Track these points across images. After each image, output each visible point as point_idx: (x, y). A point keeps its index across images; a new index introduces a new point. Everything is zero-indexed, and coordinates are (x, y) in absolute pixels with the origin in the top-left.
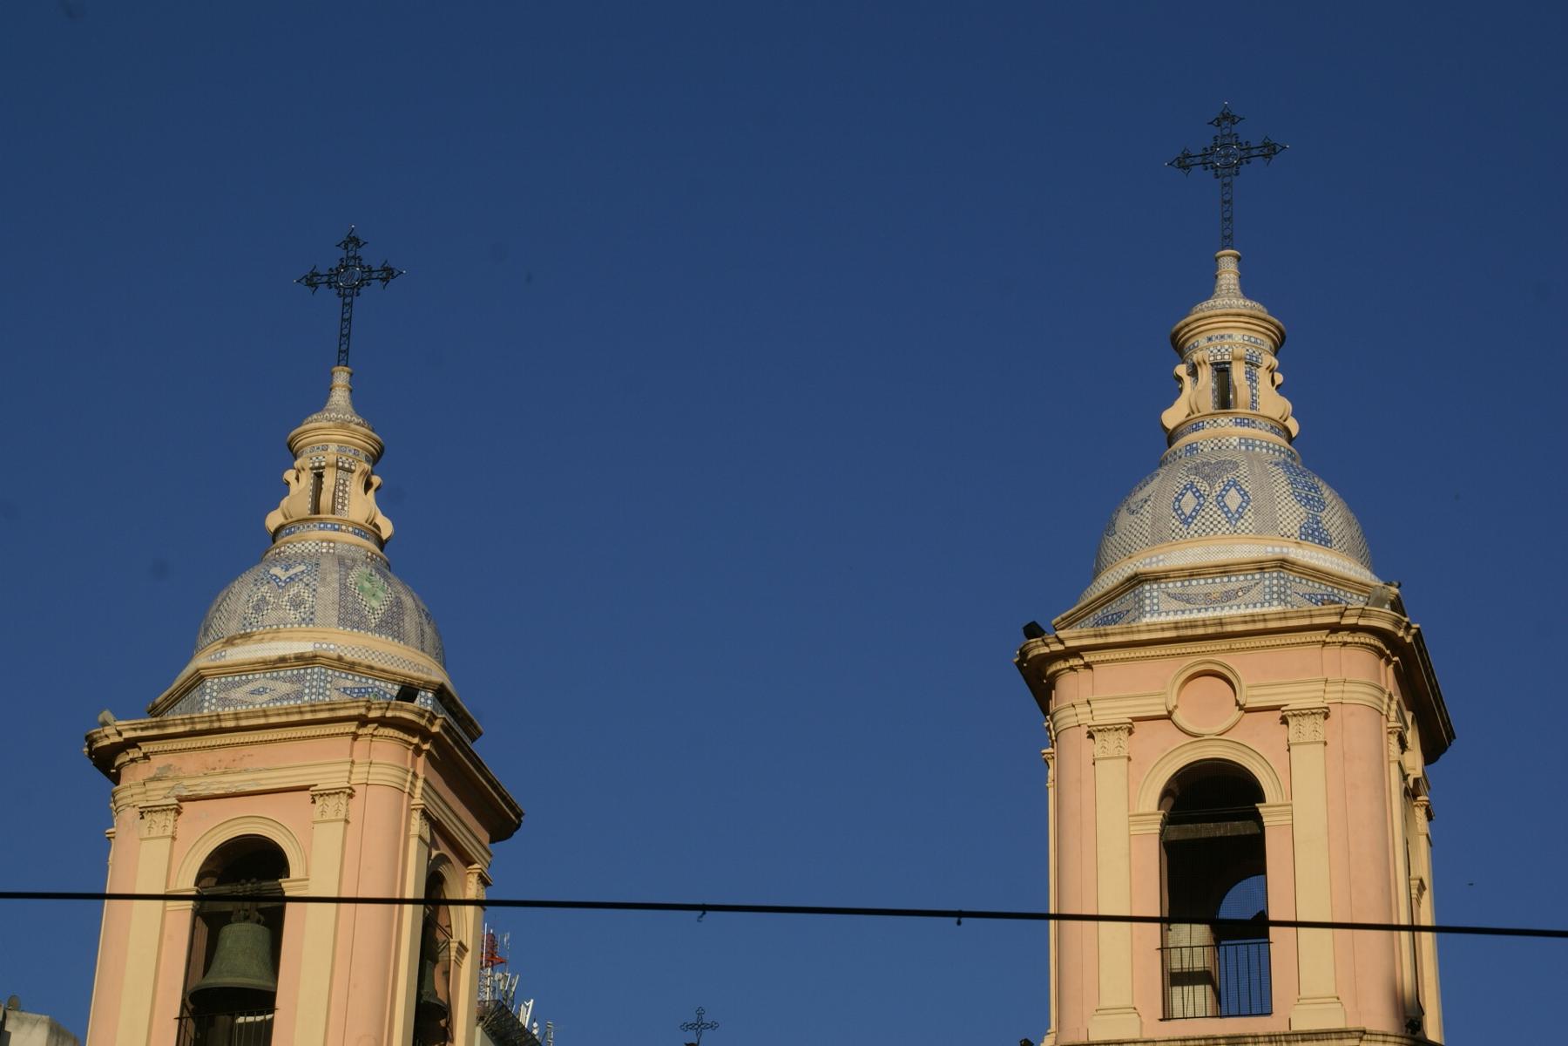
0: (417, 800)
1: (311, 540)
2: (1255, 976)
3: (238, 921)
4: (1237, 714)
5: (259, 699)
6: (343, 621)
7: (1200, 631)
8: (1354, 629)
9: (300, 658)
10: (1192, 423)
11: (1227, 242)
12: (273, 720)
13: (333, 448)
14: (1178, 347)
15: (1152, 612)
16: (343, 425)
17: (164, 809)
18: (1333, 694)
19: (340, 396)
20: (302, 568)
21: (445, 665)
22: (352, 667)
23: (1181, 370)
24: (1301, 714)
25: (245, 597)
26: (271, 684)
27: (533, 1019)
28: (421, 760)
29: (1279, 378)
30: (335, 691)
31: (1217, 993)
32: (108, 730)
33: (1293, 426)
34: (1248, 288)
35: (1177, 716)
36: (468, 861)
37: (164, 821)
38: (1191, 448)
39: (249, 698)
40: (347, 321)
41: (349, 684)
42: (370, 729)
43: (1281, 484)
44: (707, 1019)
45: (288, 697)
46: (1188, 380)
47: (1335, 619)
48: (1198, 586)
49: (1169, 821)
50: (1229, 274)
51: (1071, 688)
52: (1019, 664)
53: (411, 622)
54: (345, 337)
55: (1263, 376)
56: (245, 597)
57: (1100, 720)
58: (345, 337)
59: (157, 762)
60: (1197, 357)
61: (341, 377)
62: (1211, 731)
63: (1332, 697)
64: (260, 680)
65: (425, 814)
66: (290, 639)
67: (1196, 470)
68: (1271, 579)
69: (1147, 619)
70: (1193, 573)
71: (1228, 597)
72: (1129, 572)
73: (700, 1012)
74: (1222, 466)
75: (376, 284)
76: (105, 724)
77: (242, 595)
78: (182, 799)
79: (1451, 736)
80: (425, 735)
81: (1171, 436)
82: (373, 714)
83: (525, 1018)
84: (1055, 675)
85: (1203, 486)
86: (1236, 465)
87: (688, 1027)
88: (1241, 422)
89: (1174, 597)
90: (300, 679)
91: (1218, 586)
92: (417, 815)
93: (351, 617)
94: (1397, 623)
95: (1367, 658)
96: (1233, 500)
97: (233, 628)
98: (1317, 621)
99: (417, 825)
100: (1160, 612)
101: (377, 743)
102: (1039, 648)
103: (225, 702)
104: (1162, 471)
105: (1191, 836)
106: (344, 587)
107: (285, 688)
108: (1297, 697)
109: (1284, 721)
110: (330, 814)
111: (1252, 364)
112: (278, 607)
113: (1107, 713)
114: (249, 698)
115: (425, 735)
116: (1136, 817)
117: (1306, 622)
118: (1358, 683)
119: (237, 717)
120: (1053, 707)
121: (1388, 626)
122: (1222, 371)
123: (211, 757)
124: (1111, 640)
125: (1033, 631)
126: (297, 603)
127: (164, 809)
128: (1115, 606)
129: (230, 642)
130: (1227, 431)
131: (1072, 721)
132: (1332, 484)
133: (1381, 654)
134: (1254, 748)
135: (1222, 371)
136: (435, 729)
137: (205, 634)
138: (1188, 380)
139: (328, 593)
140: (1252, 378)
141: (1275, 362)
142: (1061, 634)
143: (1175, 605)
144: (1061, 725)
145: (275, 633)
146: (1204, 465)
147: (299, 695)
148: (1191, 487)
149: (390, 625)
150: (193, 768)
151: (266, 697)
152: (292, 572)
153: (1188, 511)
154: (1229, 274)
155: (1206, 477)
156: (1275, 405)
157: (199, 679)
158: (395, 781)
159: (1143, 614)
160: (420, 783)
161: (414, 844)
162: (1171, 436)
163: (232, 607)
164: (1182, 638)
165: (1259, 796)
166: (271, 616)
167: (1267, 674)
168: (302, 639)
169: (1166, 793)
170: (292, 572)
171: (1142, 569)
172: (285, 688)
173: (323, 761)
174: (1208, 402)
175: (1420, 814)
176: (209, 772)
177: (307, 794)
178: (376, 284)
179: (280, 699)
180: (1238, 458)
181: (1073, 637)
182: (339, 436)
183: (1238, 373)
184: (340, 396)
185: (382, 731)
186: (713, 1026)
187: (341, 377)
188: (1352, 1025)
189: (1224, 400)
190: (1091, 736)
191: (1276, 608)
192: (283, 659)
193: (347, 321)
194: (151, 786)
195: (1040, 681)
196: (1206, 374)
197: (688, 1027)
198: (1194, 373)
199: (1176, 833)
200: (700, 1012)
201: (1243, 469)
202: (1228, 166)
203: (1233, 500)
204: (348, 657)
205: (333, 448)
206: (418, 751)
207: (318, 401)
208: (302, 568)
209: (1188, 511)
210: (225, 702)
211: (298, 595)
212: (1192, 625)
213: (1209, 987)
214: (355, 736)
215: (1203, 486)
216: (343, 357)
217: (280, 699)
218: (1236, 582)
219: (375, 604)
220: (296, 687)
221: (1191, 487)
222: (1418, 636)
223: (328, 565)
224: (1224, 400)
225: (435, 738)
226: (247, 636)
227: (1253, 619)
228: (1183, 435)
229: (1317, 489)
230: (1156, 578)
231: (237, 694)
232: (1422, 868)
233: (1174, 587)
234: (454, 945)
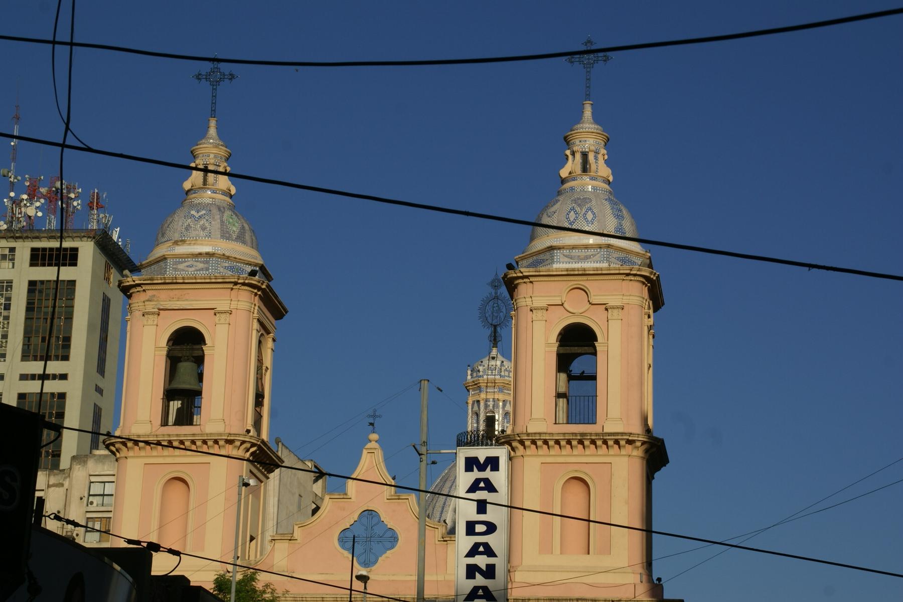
0: (256, 315)
1: (207, 196)
2: (591, 414)
3: (185, 361)
4: (588, 305)
5: (190, 269)
6: (223, 237)
7: (576, 273)
8: (635, 275)
9: (207, 254)
10: (572, 177)
11: (588, 97)
12: (199, 281)
13: (212, 156)
14: (567, 141)
15: (557, 262)
16: (216, 146)
17: (153, 313)
18: (626, 300)
19: (212, 131)
20: (204, 212)
21: (258, 249)
22: (228, 258)
23: (568, 152)
24: (613, 308)
25: (180, 223)
26: (195, 264)
27: (119, 237)
28: (257, 297)
29: (606, 157)
30: (221, 270)
31: (568, 401)
32: (129, 279)
33: (611, 179)
34: (596, 119)
35: (566, 305)
36: (268, 333)
37: (152, 319)
38: (572, 189)
39: (186, 269)
40: (214, 96)
41: (227, 265)
42: (238, 287)
43: (607, 207)
44: (377, 414)
45: (202, 269)
46: (570, 157)
47: (628, 272)
48: (575, 252)
49: (560, 346)
50: (588, 112)
51: (524, 290)
52: (503, 278)
53: (248, 236)
54: (213, 104)
55: (600, 157)
56: (180, 223)
57: (535, 305)
58: (213, 104)
59: (149, 293)
60: (575, 149)
61: (213, 123)
62: (578, 312)
63: (625, 301)
64: (190, 262)
65: (259, 320)
66: (202, 244)
67: (575, 201)
68: (604, 252)
69: (555, 266)
70: (574, 247)
71: (586, 258)
72: (548, 244)
73: (375, 411)
74: (586, 200)
75: (227, 81)
76: (127, 277)
77: (179, 222)
78: (160, 309)
79: (663, 304)
80: (259, 288)
81: (563, 181)
82: (240, 281)
83: (115, 237)
84: (518, 284)
85: (578, 209)
86: (591, 200)
87: (370, 416)
88: (592, 179)
89: (566, 256)
90: (207, 262)
91: (583, 253)
92: (255, 321)
93: (226, 235)
94: (651, 273)
95: (639, 285)
96: (590, 216)
97: (177, 236)
98: (621, 272)
99: (256, 325)
100: (560, 264)
101: (241, 292)
102: (512, 274)
103: (176, 269)
104: (561, 198)
105: (568, 352)
106: (222, 222)
107: (201, 266)
108: (612, 301)
109: (606, 309)
110: (222, 321)
111: (597, 153)
112: (196, 230)
113: (540, 302)
114: (186, 270)
115: (259, 288)
116: (548, 344)
117: (617, 272)
118: (634, 295)
119: (183, 278)
120: (515, 297)
121: (647, 274)
122: (585, 155)
123: (172, 293)
124: (541, 273)
125: (510, 267)
126: (203, 228)
127: (153, 313)
128: (541, 257)
129: (176, 243)
130: (588, 185)
131: (524, 304)
132: (630, 210)
133: (643, 283)
134: (594, 320)
135: (585, 155)
136: (264, 287)
137: (163, 235)
138: (570, 157)
139: (216, 224)
140: (596, 158)
141: (605, 152)
142: (522, 270)
143: (566, 259)
144: (519, 305)
145: (195, 241)
146: (579, 199)
147: (207, 269)
148: (573, 209)
149: (240, 238)
150: (165, 297)
151: (193, 269)
152: (200, 214)
153: (572, 219)
154: (588, 112)
155: (579, 205)
156: (605, 171)
157: (164, 259)
158: (247, 308)
159: (553, 262)
160: (257, 308)
161: (254, 332)
162: (563, 181)
163: (175, 227)
164: (569, 274)
165: (595, 338)
166: (193, 233)
167: (600, 291)
168: (207, 245)
169: (560, 334)
170: (200, 214)
171: (555, 244)
172: (201, 266)
173: (221, 299)
174: (578, 169)
175: (651, 337)
176: (171, 299)
177: (213, 311)
178: (227, 81)
179: (199, 270)
180: (592, 197)
181: (526, 272)
182: (215, 151)
183: (591, 157)
184: (212, 131)
185: (243, 287)
186: (380, 416)
187: (213, 123)
188: (626, 431)
189: (585, 168)
190: (531, 310)
191: (605, 265)
192: (200, 254)
193: (214, 96)
194: (147, 303)
195: (511, 286)
196: (578, 156)
197: (370, 416)
198: (573, 154)
199: (564, 350)
200: (375, 411)
201: (594, 202)
202: (589, 63)
203: (590, 216)
204: (227, 254)
205: (212, 156)
206: (256, 294)
207: (203, 134)
208: (204, 212)
209: (572, 219)
210: (176, 269)
211: (203, 225)
212: (573, 270)
213: (565, 400)
214: (232, 289)
215: (578, 209)
216: (213, 114)
217: (199, 270)
218: (590, 252)
219: (235, 229)
220: (206, 265)
221: (573, 209)
222: (658, 277)
223: (215, 211)
224: (585, 168)
225: (263, 290)
226: (183, 241)
227: (597, 269)
228: (568, 181)
229: (620, 210)
230: (559, 248)
231: (181, 266)
232: (651, 362)
233: (566, 252)
234: (264, 368)
